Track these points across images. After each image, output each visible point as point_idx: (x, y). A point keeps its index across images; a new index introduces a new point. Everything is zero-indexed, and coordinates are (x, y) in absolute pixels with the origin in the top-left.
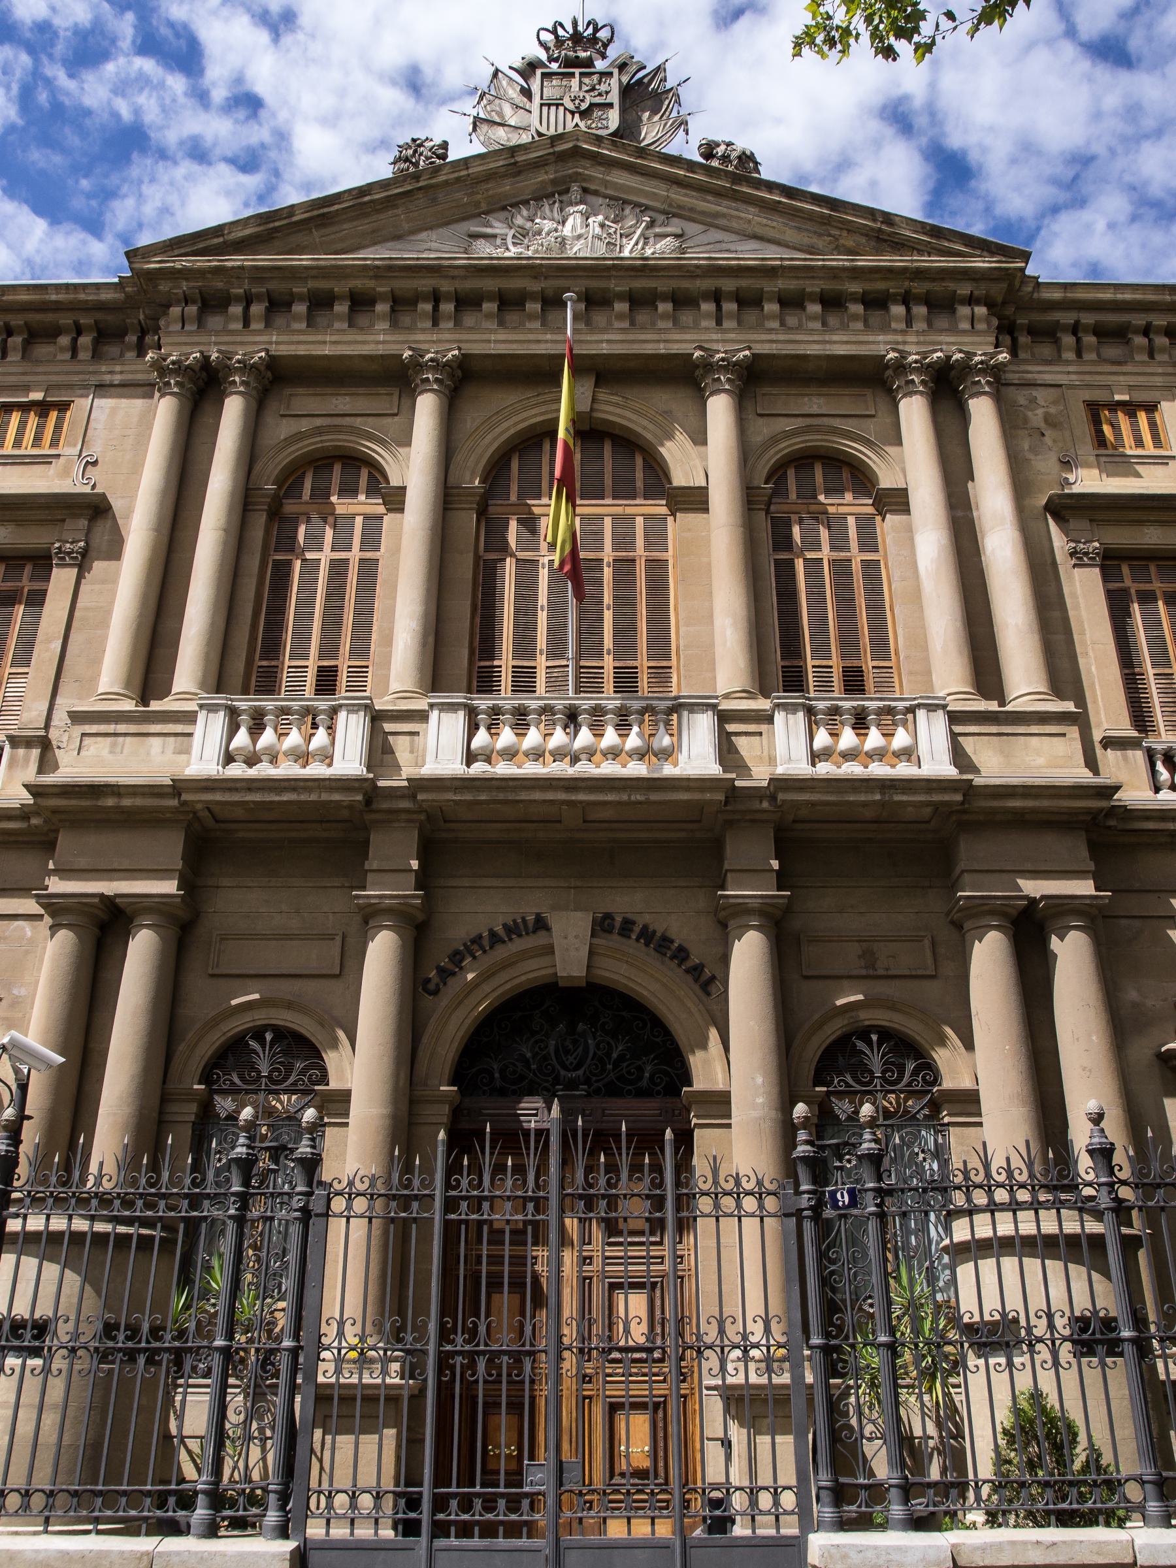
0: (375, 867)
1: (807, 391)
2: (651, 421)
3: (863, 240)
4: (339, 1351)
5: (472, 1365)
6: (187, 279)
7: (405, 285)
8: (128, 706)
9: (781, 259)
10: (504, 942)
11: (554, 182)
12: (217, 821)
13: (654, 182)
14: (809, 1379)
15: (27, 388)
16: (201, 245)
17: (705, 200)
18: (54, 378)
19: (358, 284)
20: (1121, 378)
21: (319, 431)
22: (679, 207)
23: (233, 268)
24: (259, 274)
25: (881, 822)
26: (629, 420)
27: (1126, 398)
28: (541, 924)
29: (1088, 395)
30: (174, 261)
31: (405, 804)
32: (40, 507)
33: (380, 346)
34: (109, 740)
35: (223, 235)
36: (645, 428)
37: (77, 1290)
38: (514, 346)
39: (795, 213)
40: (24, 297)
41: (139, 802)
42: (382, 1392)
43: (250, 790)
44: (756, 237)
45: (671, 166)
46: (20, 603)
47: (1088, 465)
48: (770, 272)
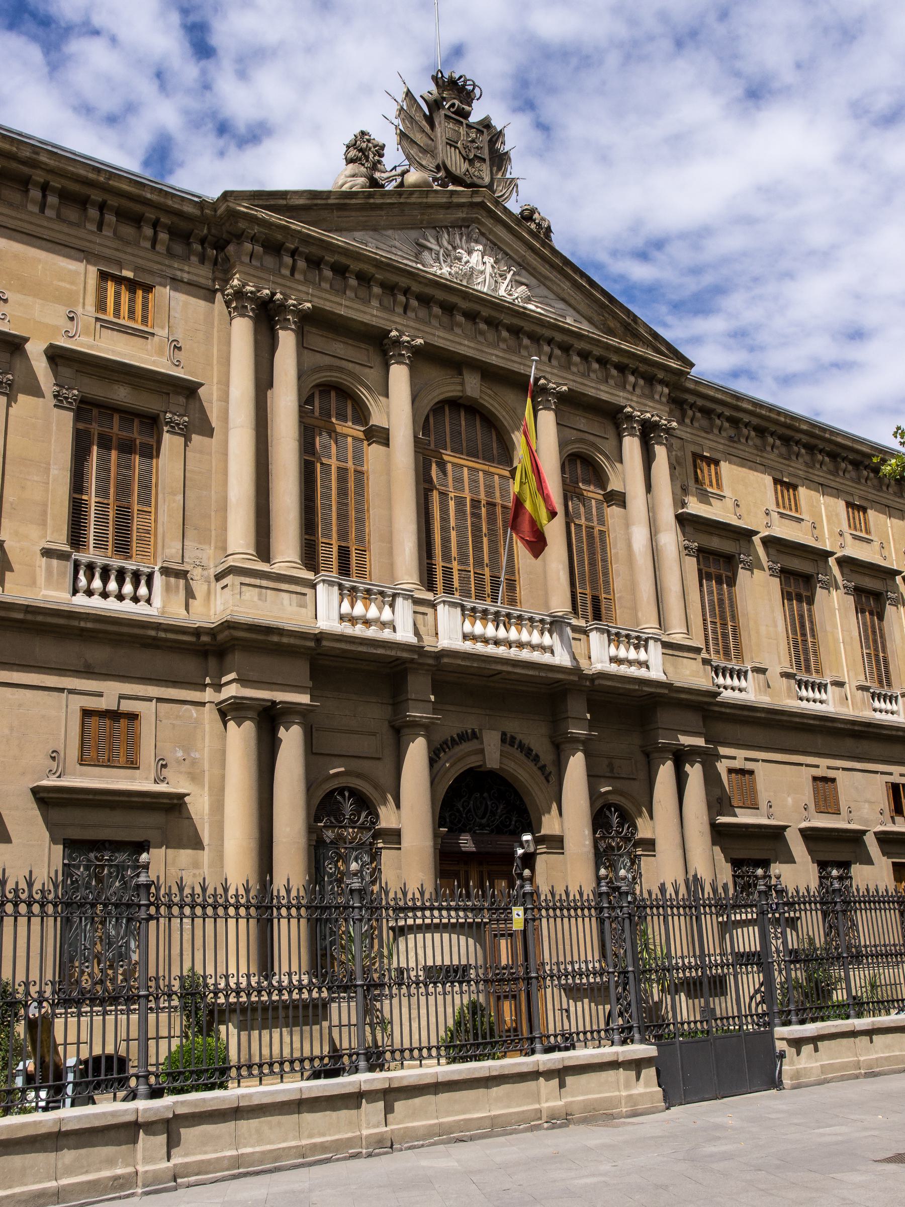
0: (413, 697)
1: (577, 412)
2: (507, 413)
3: (618, 325)
6: (258, 225)
9: (588, 331)
11: (464, 219)
13: (519, 243)
15: (120, 265)
16: (272, 202)
17: (544, 267)
18: (140, 261)
20: (707, 442)
21: (330, 368)
22: (528, 264)
23: (295, 230)
24: (307, 239)
26: (496, 408)
27: (708, 455)
28: (474, 736)
29: (697, 450)
30: (257, 211)
31: (431, 661)
32: (159, 381)
33: (374, 319)
34: (257, 590)
35: (286, 199)
36: (504, 417)
38: (448, 343)
39: (590, 296)
40: (125, 187)
41: (292, 641)
43: (361, 644)
44: (563, 300)
45: (533, 238)
46: (135, 453)
47: (693, 495)
48: (579, 336)
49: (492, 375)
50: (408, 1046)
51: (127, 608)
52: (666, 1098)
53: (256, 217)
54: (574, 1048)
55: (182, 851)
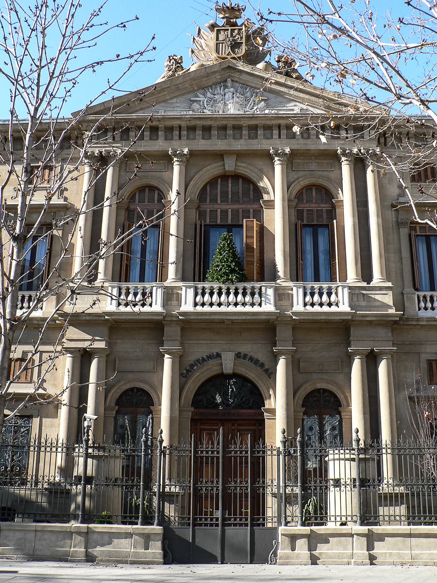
5: (212, 489)
7: (169, 123)
10: (206, 361)
12: (116, 322)
14: (281, 492)
25: (327, 323)
28: (218, 355)
42: (175, 494)
49: (240, 155)
51: (256, 309)
52: (165, 556)
55: (48, 419)
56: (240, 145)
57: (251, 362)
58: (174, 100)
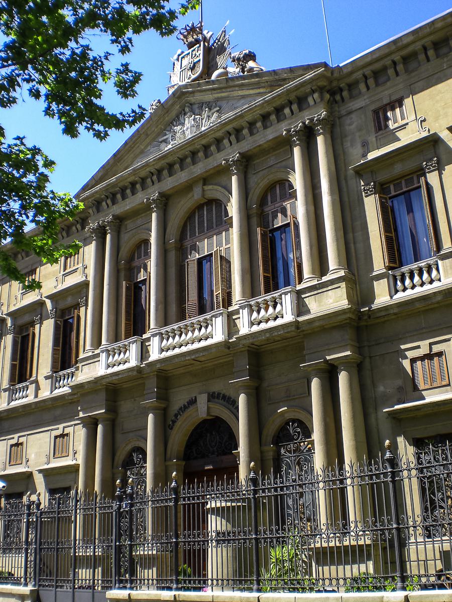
4: (356, 532)
8: (315, 282)
19: (235, 124)
29: (373, 107)
37: (220, 520)
50: (151, 578)
51: (428, 288)
53: (87, 196)
54: (385, 590)
56: (199, 169)
57: (224, 401)
58: (149, 148)
